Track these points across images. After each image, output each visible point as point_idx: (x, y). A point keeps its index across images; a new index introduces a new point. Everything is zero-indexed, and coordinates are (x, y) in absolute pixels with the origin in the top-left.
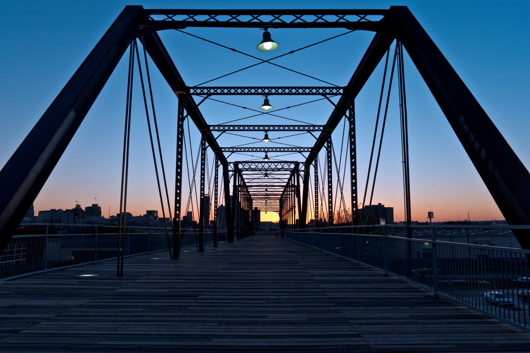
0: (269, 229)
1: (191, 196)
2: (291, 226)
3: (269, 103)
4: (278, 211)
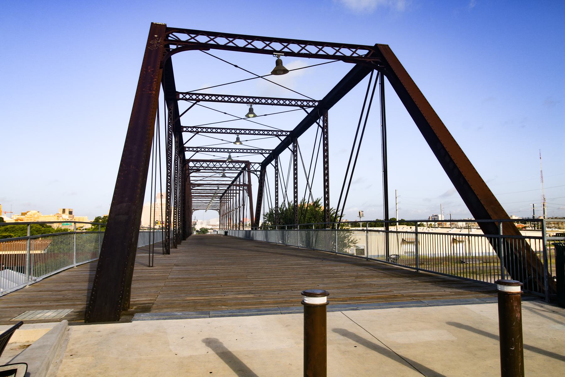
1: (286, 189)
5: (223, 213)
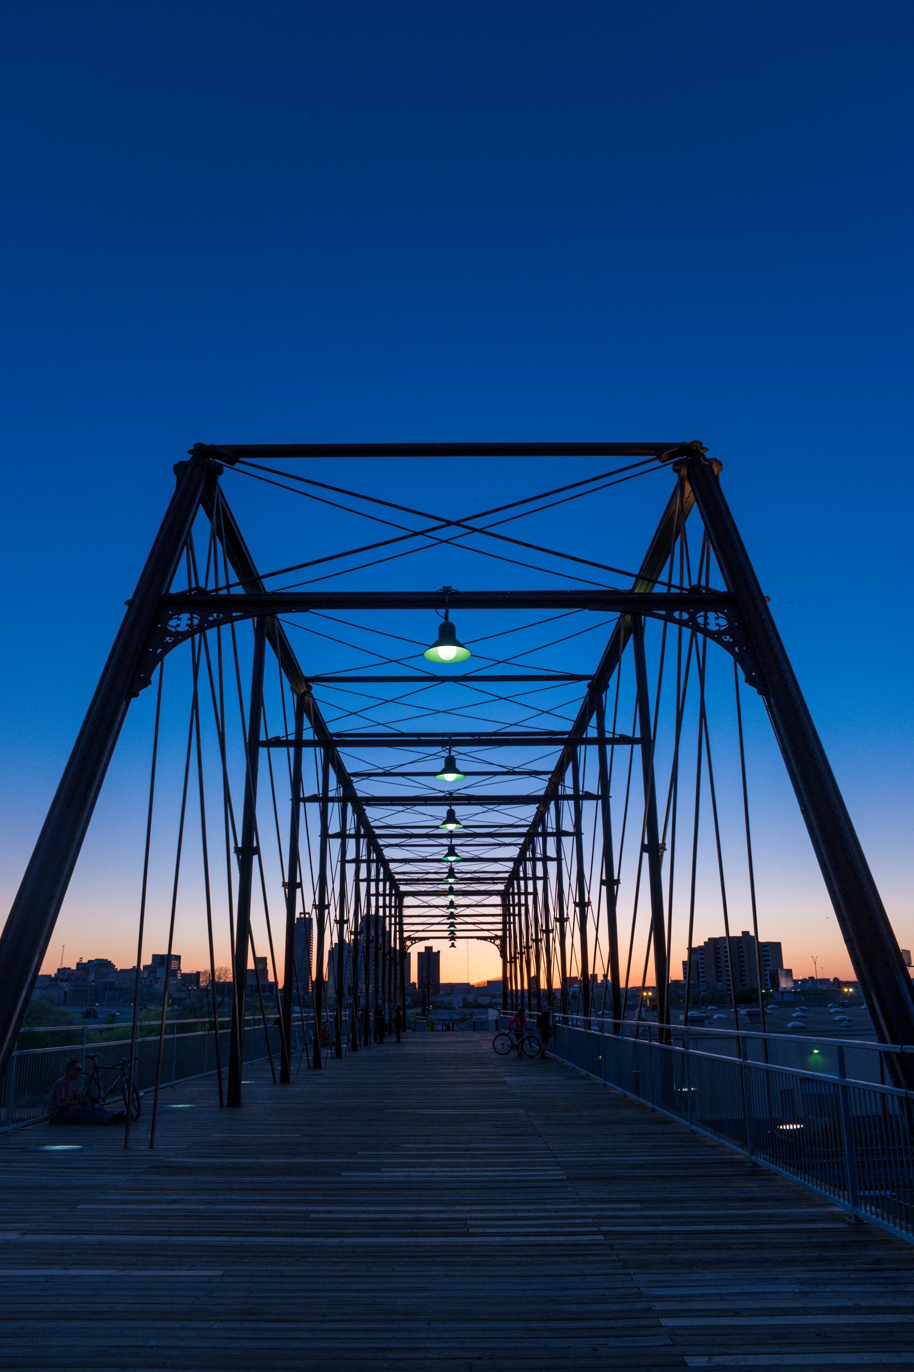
0: (461, 1005)
2: (519, 994)
3: (457, 767)
4: (496, 937)
5: (516, 947)
